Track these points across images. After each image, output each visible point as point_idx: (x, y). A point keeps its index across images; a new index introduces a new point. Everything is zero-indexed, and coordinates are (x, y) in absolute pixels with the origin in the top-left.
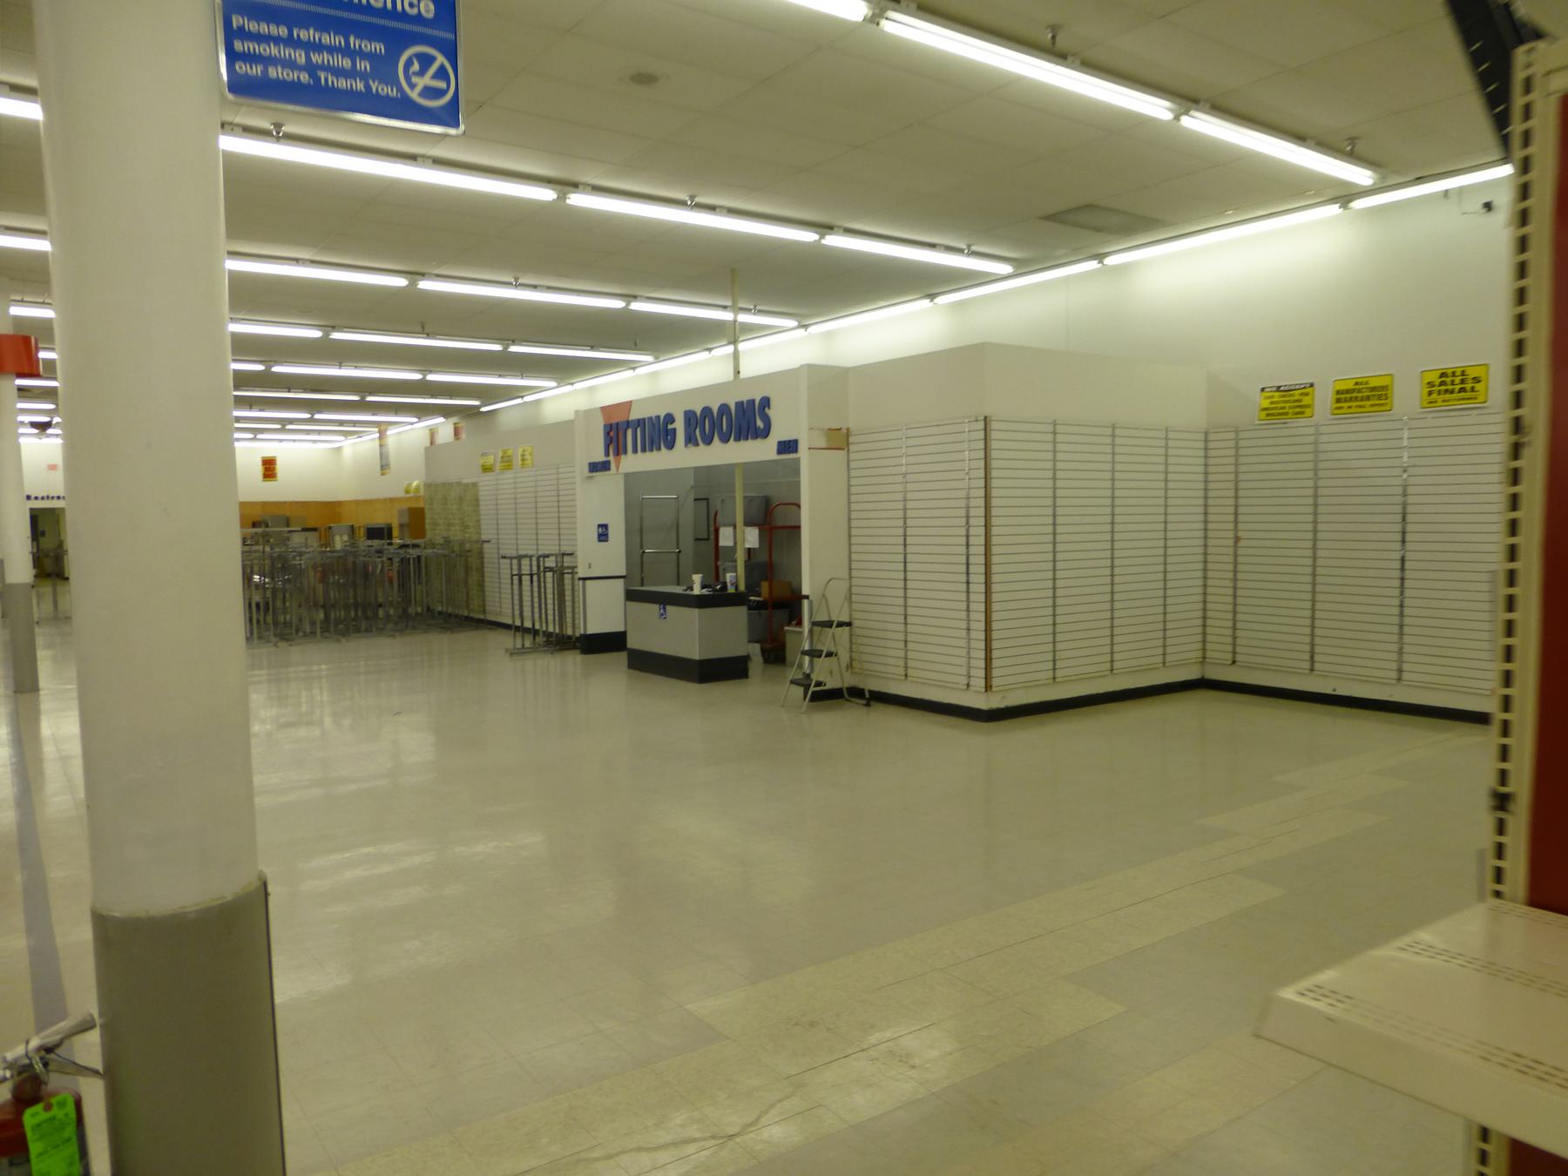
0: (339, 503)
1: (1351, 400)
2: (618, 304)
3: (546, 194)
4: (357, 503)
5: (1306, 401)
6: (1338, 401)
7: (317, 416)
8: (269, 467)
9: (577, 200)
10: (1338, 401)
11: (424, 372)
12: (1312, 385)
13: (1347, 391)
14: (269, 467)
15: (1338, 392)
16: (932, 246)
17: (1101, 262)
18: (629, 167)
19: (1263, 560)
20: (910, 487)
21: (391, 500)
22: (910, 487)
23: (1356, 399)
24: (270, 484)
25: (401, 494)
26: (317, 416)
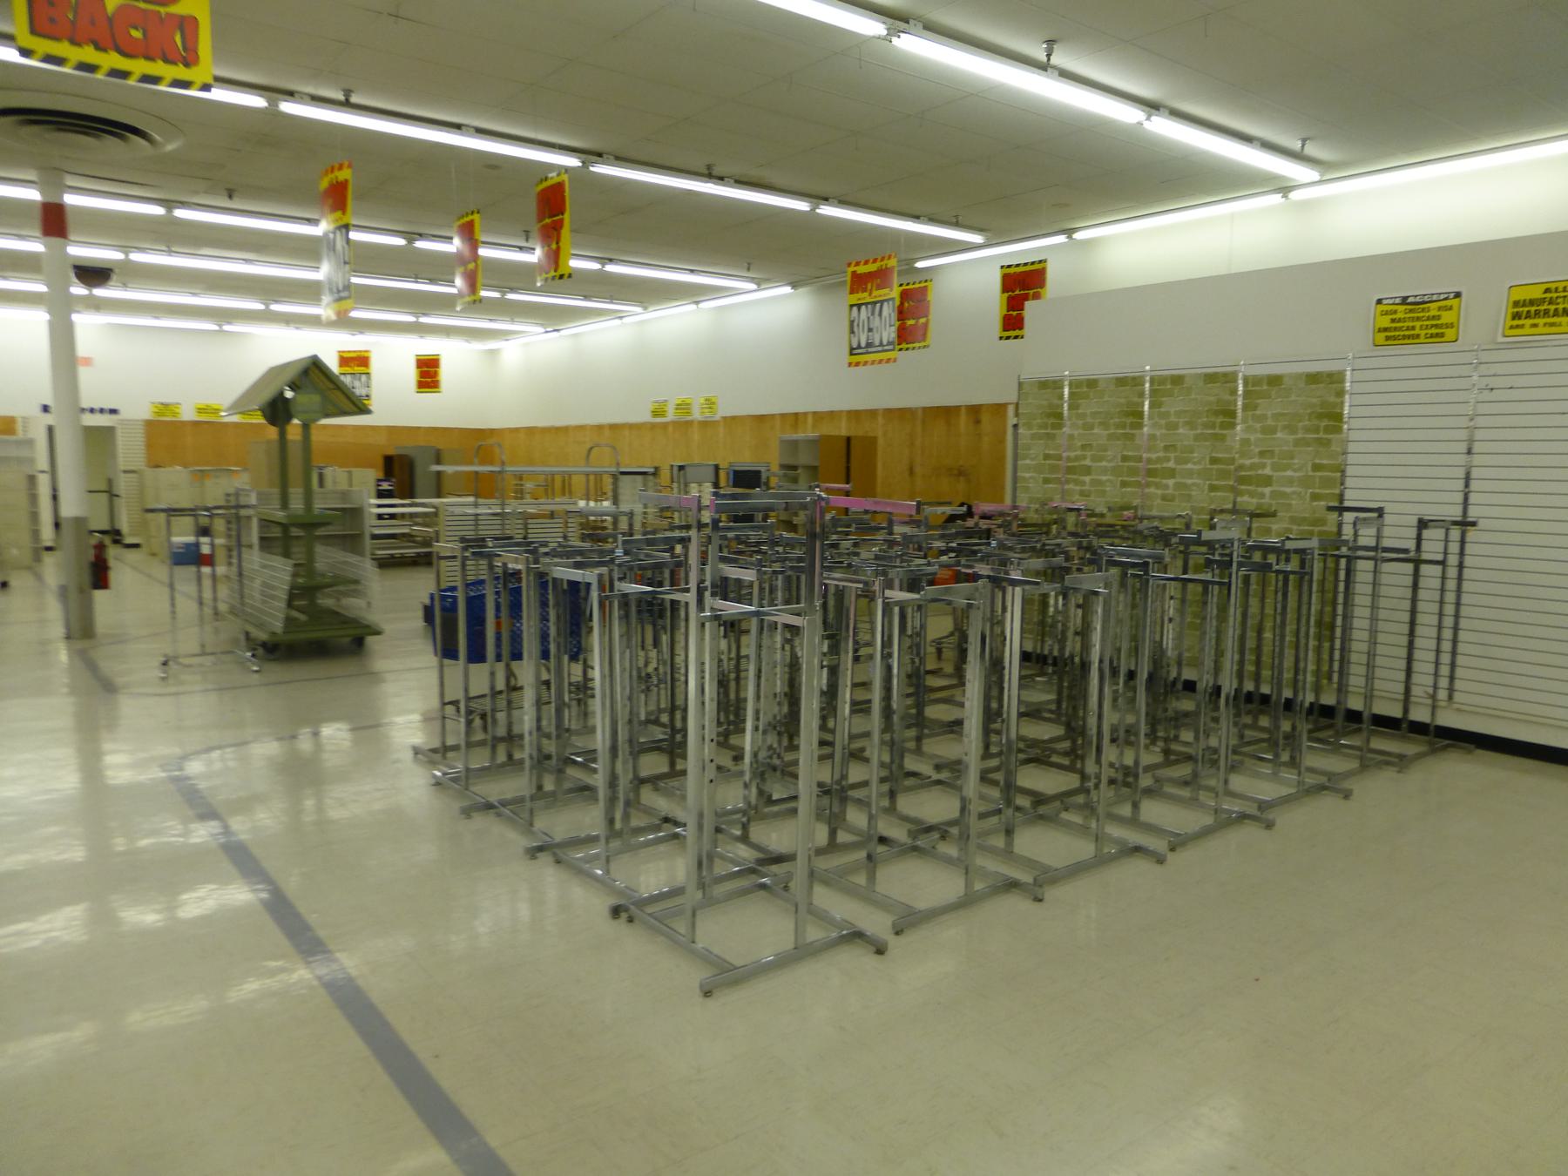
0: (492, 432)
1: (1537, 313)
2: (595, 266)
3: (257, 101)
4: (531, 431)
5: (1447, 317)
6: (1516, 316)
7: (275, 307)
8: (428, 373)
9: (287, 107)
10: (1516, 316)
11: (125, 249)
12: (1458, 295)
13: (1532, 302)
14: (428, 373)
15: (1516, 304)
16: (457, 127)
17: (1285, 196)
18: (507, 108)
19: (1483, 676)
20: (1480, 421)
21: (761, 419)
22: (1480, 421)
23: (1546, 312)
24: (428, 397)
25: (644, 416)
26: (275, 307)
